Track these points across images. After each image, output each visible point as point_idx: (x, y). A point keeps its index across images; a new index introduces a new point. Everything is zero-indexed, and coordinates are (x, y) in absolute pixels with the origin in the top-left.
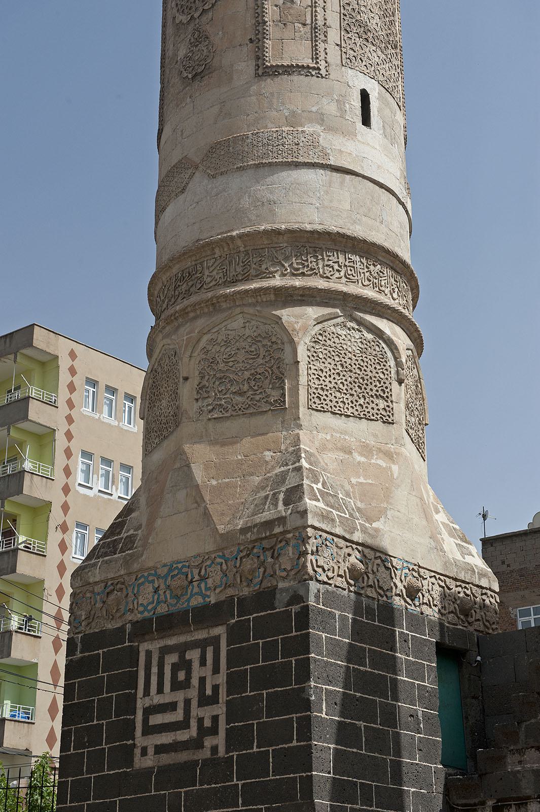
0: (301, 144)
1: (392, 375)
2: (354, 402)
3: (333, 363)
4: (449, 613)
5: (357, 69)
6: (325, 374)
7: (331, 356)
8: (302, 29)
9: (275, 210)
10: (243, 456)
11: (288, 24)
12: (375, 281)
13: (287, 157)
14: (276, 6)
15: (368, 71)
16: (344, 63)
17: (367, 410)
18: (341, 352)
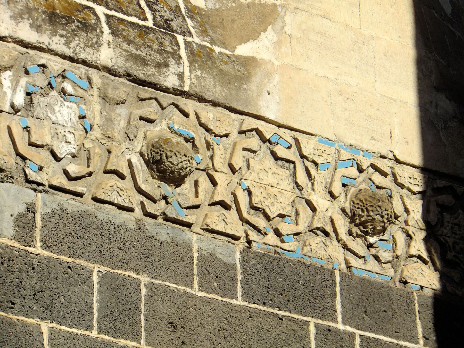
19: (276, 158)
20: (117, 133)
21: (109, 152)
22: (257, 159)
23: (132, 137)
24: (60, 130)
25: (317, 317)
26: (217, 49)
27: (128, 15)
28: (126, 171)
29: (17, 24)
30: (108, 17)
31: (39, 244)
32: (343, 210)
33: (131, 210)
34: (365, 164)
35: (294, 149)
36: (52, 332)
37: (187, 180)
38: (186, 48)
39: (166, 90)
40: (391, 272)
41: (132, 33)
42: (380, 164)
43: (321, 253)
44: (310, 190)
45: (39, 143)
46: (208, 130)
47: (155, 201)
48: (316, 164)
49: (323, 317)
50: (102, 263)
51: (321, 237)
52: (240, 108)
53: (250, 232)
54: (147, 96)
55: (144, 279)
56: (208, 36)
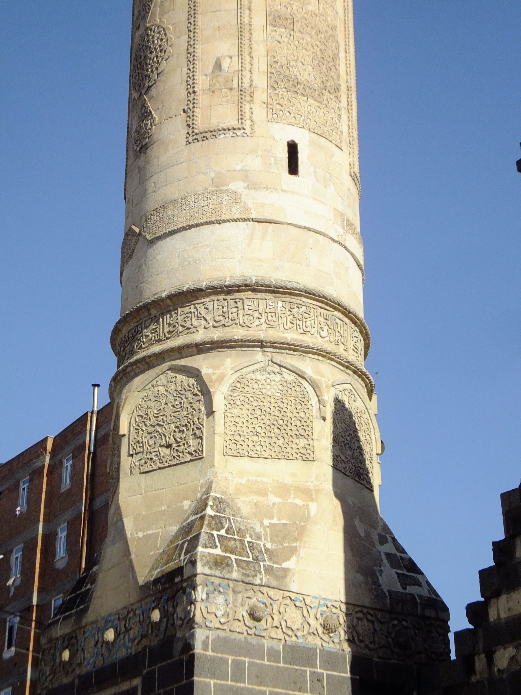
0: (224, 203)
1: (314, 413)
2: (272, 444)
3: (251, 408)
4: (380, 647)
5: (285, 122)
6: (242, 420)
7: (249, 402)
8: (229, 93)
9: (199, 268)
10: (166, 507)
11: (216, 91)
12: (298, 322)
13: (210, 217)
14: (206, 75)
15: (297, 122)
16: (270, 119)
17: (285, 451)
18: (260, 397)
19: (296, 606)
20: (238, 604)
21: (235, 612)
22: (289, 608)
23: (243, 605)
24: (218, 606)
25: (310, 667)
26: (275, 566)
27: (243, 557)
28: (241, 619)
29: (204, 568)
30: (236, 559)
31: (210, 650)
32: (321, 624)
33: (243, 633)
34: (329, 604)
35: (303, 602)
36: (214, 684)
37: (263, 619)
38: (264, 568)
39: (256, 585)
40: (338, 647)
41: (244, 564)
42: (335, 604)
43: (312, 642)
44: (309, 618)
45: (211, 612)
46: (271, 598)
47: (251, 629)
48: (311, 607)
49: (312, 667)
50: (232, 655)
51: (313, 635)
52: (283, 589)
53: (286, 637)
54: (249, 588)
55: (247, 660)
56: (272, 560)
